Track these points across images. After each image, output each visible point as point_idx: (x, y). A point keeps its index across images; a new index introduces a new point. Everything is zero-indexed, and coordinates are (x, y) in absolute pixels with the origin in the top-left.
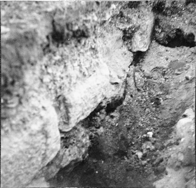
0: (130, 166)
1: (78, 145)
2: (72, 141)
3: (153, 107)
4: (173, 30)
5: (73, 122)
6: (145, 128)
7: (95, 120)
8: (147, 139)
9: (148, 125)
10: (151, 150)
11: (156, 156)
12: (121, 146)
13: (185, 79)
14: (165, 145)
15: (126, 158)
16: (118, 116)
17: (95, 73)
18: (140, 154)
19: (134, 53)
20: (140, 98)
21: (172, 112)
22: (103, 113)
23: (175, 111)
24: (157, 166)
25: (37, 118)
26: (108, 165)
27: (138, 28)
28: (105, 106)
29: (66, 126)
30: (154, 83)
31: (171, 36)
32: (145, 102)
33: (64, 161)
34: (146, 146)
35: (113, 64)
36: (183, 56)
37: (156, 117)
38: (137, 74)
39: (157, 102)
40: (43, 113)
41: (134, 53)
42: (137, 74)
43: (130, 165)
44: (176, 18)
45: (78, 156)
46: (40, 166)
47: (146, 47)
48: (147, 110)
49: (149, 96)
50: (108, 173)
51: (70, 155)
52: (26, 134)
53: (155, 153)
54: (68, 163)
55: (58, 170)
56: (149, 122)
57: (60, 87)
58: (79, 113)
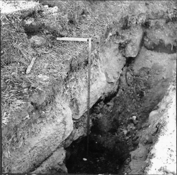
0: (118, 140)
1: (84, 126)
2: (80, 124)
3: (138, 98)
4: (157, 40)
5: (81, 113)
6: (131, 113)
7: (96, 108)
8: (132, 121)
9: (133, 111)
10: (133, 129)
11: (135, 134)
12: (113, 126)
13: (162, 78)
14: (143, 126)
15: (116, 134)
16: (113, 105)
17: (96, 81)
18: (125, 132)
19: (126, 58)
20: (129, 91)
21: (151, 102)
22: (102, 104)
23: (153, 102)
24: (135, 141)
25: (61, 115)
26: (104, 139)
27: (130, 41)
28: (103, 99)
29: (77, 116)
30: (140, 79)
31: (156, 43)
32: (132, 94)
33: (75, 136)
34: (130, 127)
35: (110, 68)
36: (162, 60)
37: (140, 105)
38: (128, 73)
39: (142, 95)
40: (63, 112)
41: (126, 58)
42: (128, 73)
43: (118, 139)
44: (158, 32)
45: (84, 133)
46: (61, 141)
47: (135, 54)
48: (134, 100)
49: (136, 90)
50: (104, 142)
51: (79, 133)
52: (54, 124)
53: (135, 132)
54: (78, 138)
55: (72, 142)
56: (134, 109)
57: (74, 94)
58: (83, 109)
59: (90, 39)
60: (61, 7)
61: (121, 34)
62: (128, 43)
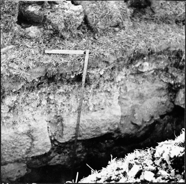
17: (103, 111)
19: (175, 106)
29: (61, 139)
33: (52, 161)
51: (58, 159)
59: (88, 52)
60: (86, 8)
61: (170, 72)
62: (181, 88)
